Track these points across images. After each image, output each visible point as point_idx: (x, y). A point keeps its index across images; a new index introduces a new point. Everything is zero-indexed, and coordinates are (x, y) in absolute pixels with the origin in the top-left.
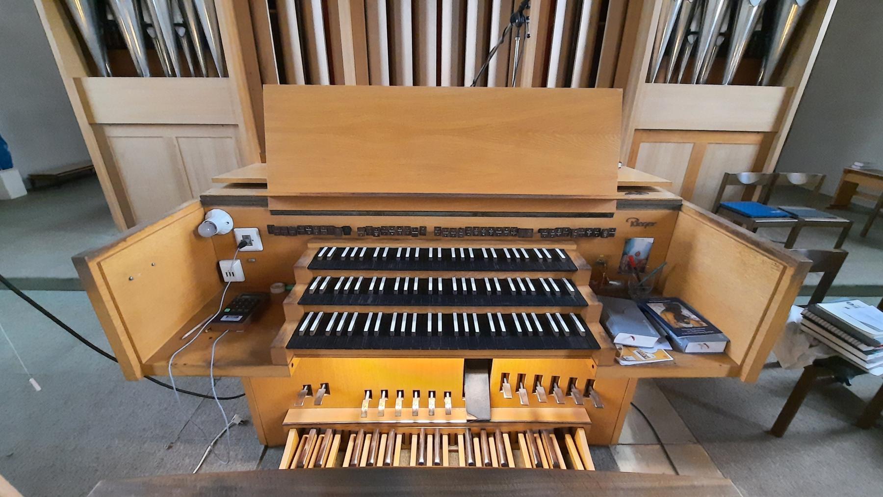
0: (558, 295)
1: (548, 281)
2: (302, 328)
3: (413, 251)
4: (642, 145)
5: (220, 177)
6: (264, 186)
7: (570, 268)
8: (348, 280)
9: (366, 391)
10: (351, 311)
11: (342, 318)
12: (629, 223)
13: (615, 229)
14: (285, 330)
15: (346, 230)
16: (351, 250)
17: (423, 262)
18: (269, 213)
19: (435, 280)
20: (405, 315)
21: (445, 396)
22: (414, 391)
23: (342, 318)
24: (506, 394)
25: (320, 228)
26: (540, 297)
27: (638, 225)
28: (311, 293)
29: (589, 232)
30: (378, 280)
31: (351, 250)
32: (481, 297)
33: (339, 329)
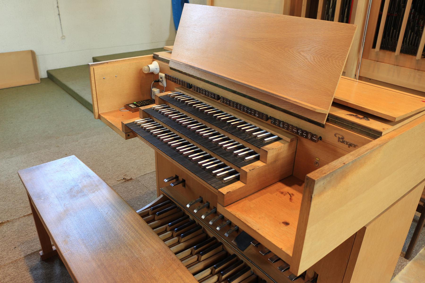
27: (343, 142)
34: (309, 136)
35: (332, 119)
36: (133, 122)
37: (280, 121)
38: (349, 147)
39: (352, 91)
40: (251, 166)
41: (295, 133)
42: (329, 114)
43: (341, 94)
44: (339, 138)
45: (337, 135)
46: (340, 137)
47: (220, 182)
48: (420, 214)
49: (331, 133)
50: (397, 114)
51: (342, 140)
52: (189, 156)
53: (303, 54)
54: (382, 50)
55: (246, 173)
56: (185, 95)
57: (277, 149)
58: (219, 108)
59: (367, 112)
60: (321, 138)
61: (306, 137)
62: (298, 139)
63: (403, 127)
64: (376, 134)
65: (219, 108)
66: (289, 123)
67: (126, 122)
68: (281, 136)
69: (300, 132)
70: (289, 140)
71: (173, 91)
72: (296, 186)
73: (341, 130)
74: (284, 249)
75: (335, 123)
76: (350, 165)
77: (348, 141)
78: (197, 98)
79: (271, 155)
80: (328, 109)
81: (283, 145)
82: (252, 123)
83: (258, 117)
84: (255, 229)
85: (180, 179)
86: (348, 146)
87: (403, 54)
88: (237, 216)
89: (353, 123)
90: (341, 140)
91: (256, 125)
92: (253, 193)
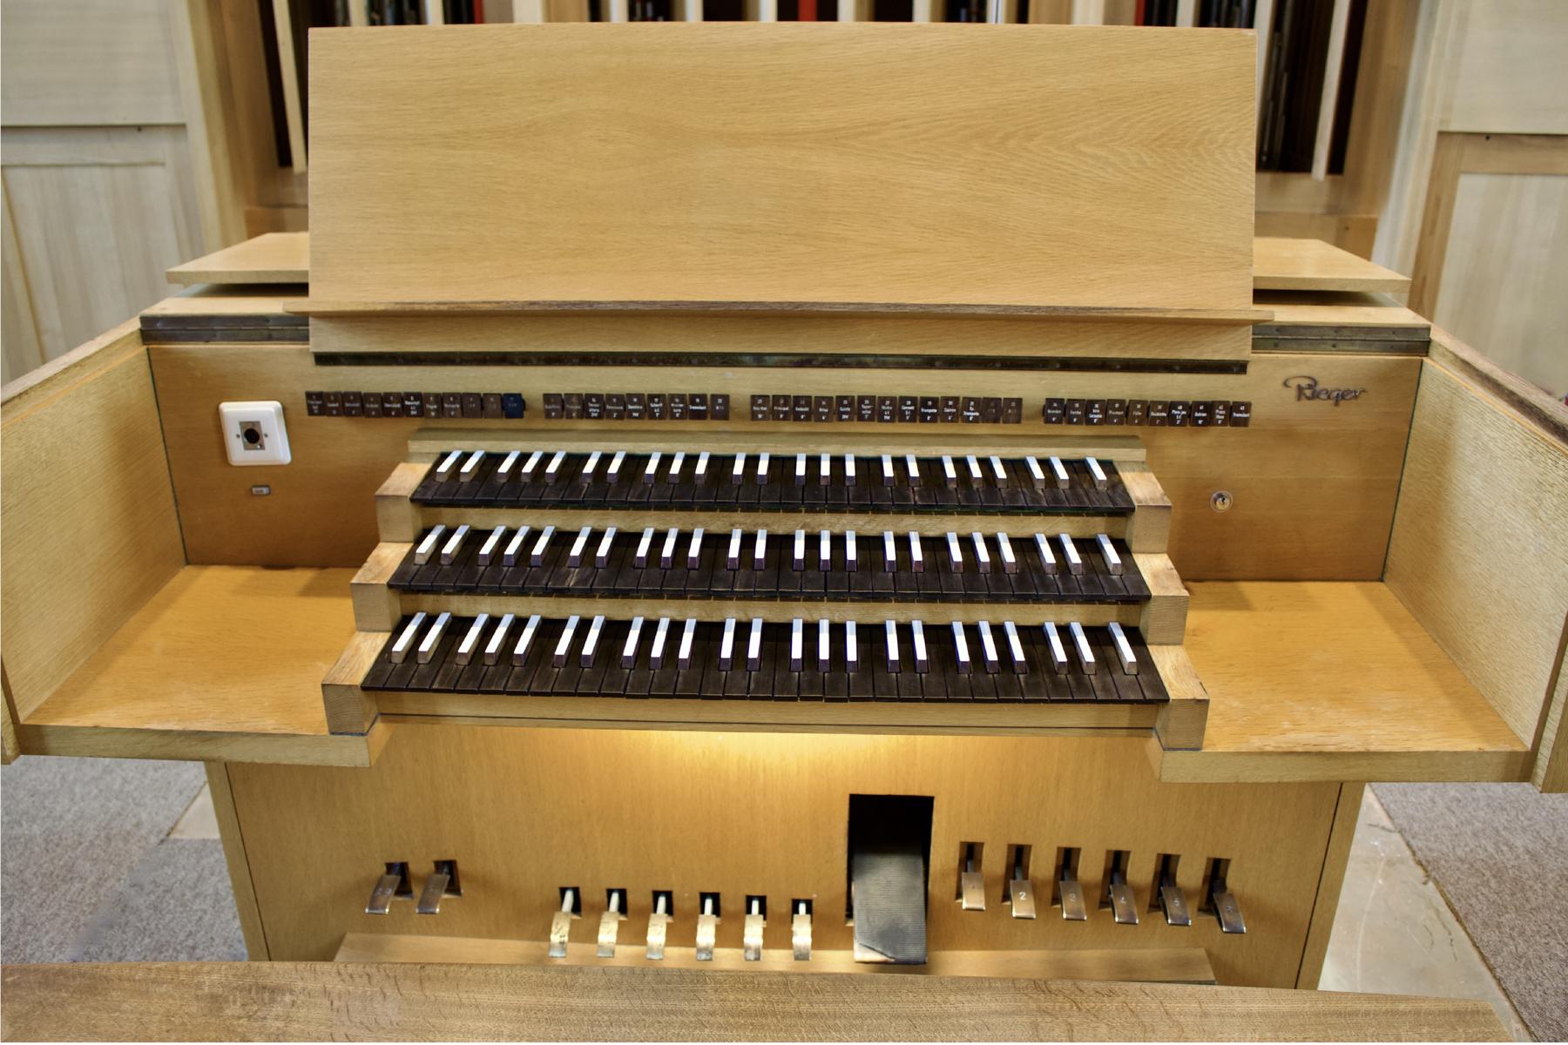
0: (1077, 574)
1: (1056, 537)
2: (401, 645)
3: (691, 461)
4: (1465, 182)
5: (190, 267)
6: (300, 289)
7: (1120, 508)
8: (511, 530)
9: (563, 891)
10: (523, 613)
11: (497, 622)
12: (1293, 393)
13: (1248, 406)
14: (358, 649)
15: (512, 406)
16: (523, 458)
17: (717, 488)
18: (312, 360)
19: (748, 533)
20: (664, 625)
21: (795, 910)
22: (704, 896)
23: (497, 622)
24: (973, 899)
25: (441, 399)
26: (1026, 580)
27: (1315, 396)
28: (439, 479)
29: (1179, 413)
30: (595, 530)
31: (523, 458)
32: (866, 576)
33: (492, 647)
35: (1270, 337)
38: (1336, 404)
44: (1300, 389)
46: (1304, 383)
48: (311, 30)
53: (1082, 147)
75: (1276, 345)
85: (421, 866)
86: (1332, 402)
89: (1339, 328)
90: (1308, 393)
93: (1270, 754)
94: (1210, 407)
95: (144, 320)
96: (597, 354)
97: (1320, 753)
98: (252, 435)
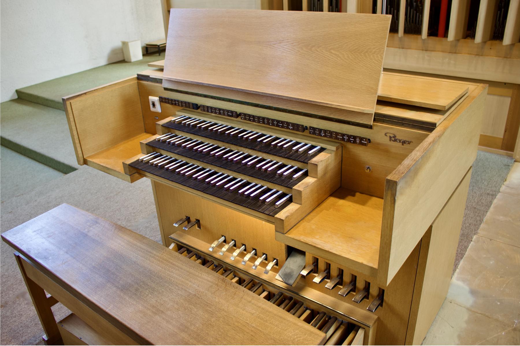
27: (395, 140)
34: (358, 141)
35: (379, 118)
36: (138, 160)
37: (320, 130)
38: (403, 145)
39: (392, 86)
40: (302, 184)
41: (341, 140)
42: (375, 113)
43: (382, 91)
44: (390, 137)
45: (387, 135)
46: (392, 136)
47: (272, 208)
49: (380, 134)
50: (442, 102)
51: (394, 138)
52: (226, 187)
53: (275, 46)
54: (406, 35)
55: (300, 192)
56: (195, 118)
57: (325, 160)
58: (240, 127)
59: (414, 105)
60: (369, 141)
61: (355, 142)
62: (343, 146)
63: (451, 115)
64: (430, 127)
65: (240, 127)
66: (332, 130)
67: (129, 161)
68: (324, 146)
69: (346, 138)
70: (334, 148)
71: (174, 115)
72: (350, 197)
73: (392, 128)
74: (365, 262)
75: (383, 122)
76: (420, 160)
77: (400, 139)
78: (209, 120)
79: (320, 168)
80: (373, 108)
81: (330, 155)
82: (286, 137)
83: (293, 129)
84: (327, 249)
85: (193, 219)
86: (401, 144)
87: (431, 37)
88: (302, 240)
90: (393, 139)
91: (292, 139)
92: (309, 214)
93: (302, 242)
94: (355, 137)
95: (138, 75)
96: (246, 102)
97: (315, 247)
98: (154, 105)
